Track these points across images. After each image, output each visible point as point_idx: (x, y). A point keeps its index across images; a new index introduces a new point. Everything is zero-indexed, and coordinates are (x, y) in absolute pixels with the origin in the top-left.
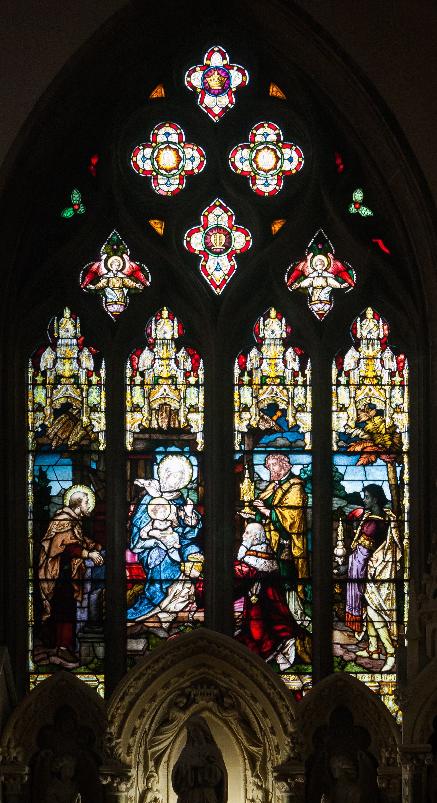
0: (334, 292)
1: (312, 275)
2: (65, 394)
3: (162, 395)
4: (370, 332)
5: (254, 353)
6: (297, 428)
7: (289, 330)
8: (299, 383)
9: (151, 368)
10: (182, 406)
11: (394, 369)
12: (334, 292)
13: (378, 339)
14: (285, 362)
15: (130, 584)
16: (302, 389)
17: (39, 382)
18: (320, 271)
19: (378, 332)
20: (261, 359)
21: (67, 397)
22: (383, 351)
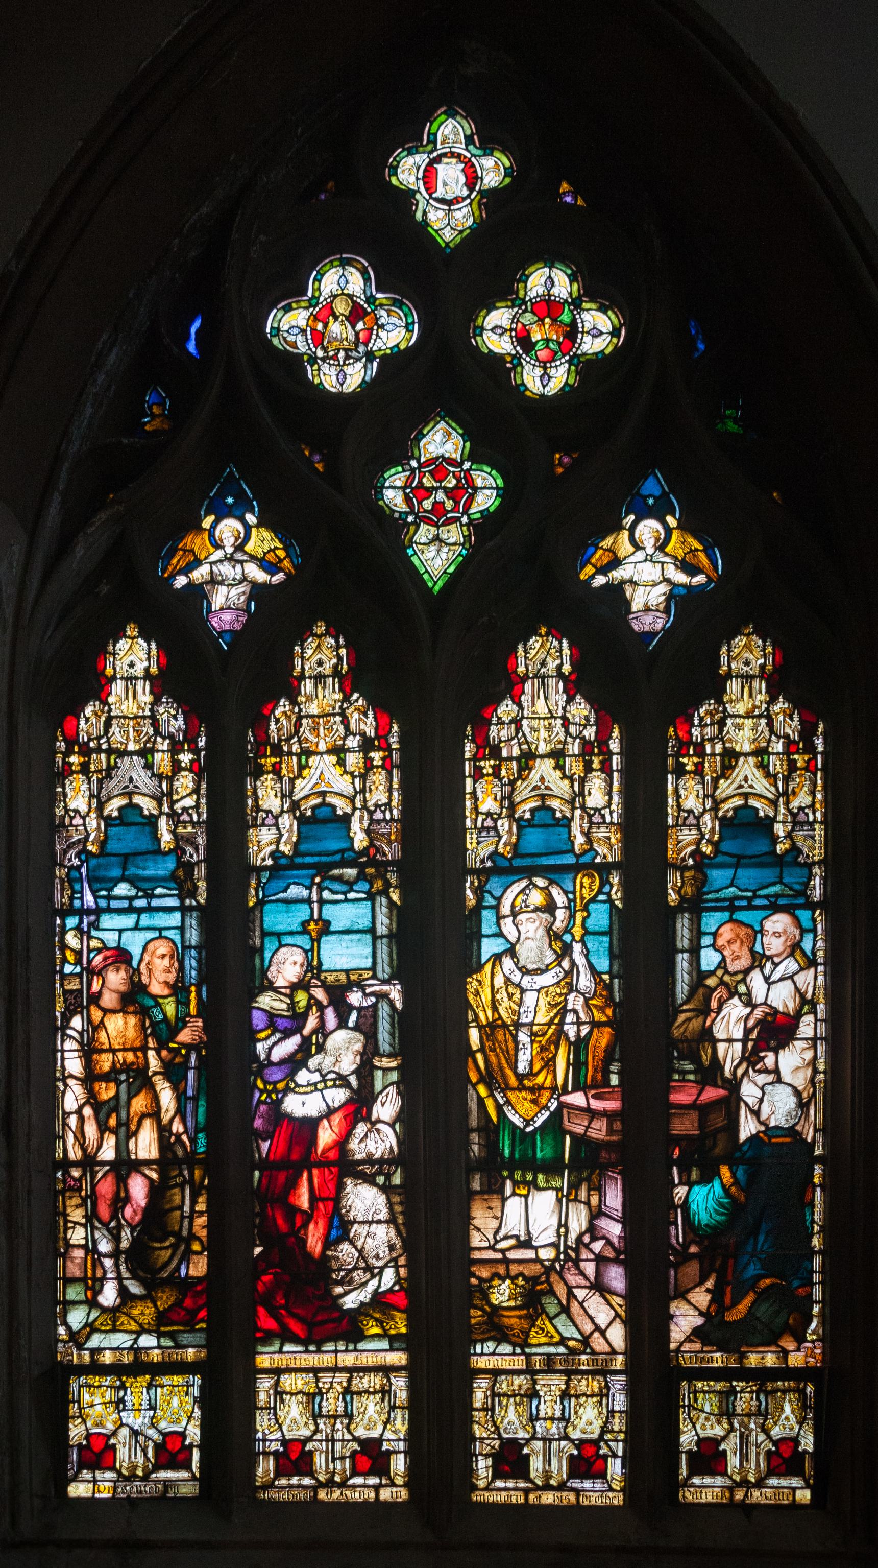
0: (257, 591)
1: (632, 559)
2: (127, 787)
3: (536, 788)
4: (132, 665)
5: (283, 707)
6: (795, 853)
7: (164, 661)
8: (375, 763)
9: (513, 739)
10: (782, 810)
11: (370, 732)
12: (257, 591)
13: (560, 675)
14: (345, 722)
15: (295, 1157)
16: (374, 774)
17: (689, 768)
18: (650, 550)
19: (762, 661)
20: (300, 718)
21: (746, 796)
22: (772, 700)
